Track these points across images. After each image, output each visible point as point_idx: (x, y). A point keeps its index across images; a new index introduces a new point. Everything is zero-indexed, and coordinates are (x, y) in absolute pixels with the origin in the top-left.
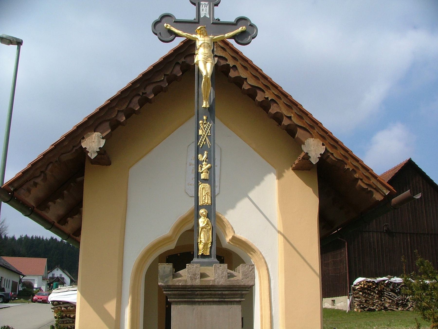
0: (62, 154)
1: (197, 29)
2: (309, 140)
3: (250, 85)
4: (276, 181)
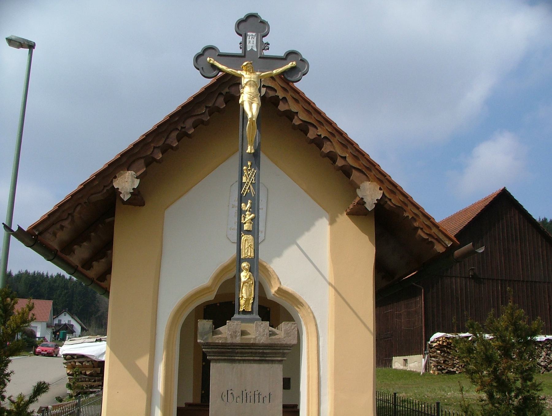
0: (92, 194)
1: (243, 65)
2: (365, 184)
3: (301, 120)
4: (328, 227)
